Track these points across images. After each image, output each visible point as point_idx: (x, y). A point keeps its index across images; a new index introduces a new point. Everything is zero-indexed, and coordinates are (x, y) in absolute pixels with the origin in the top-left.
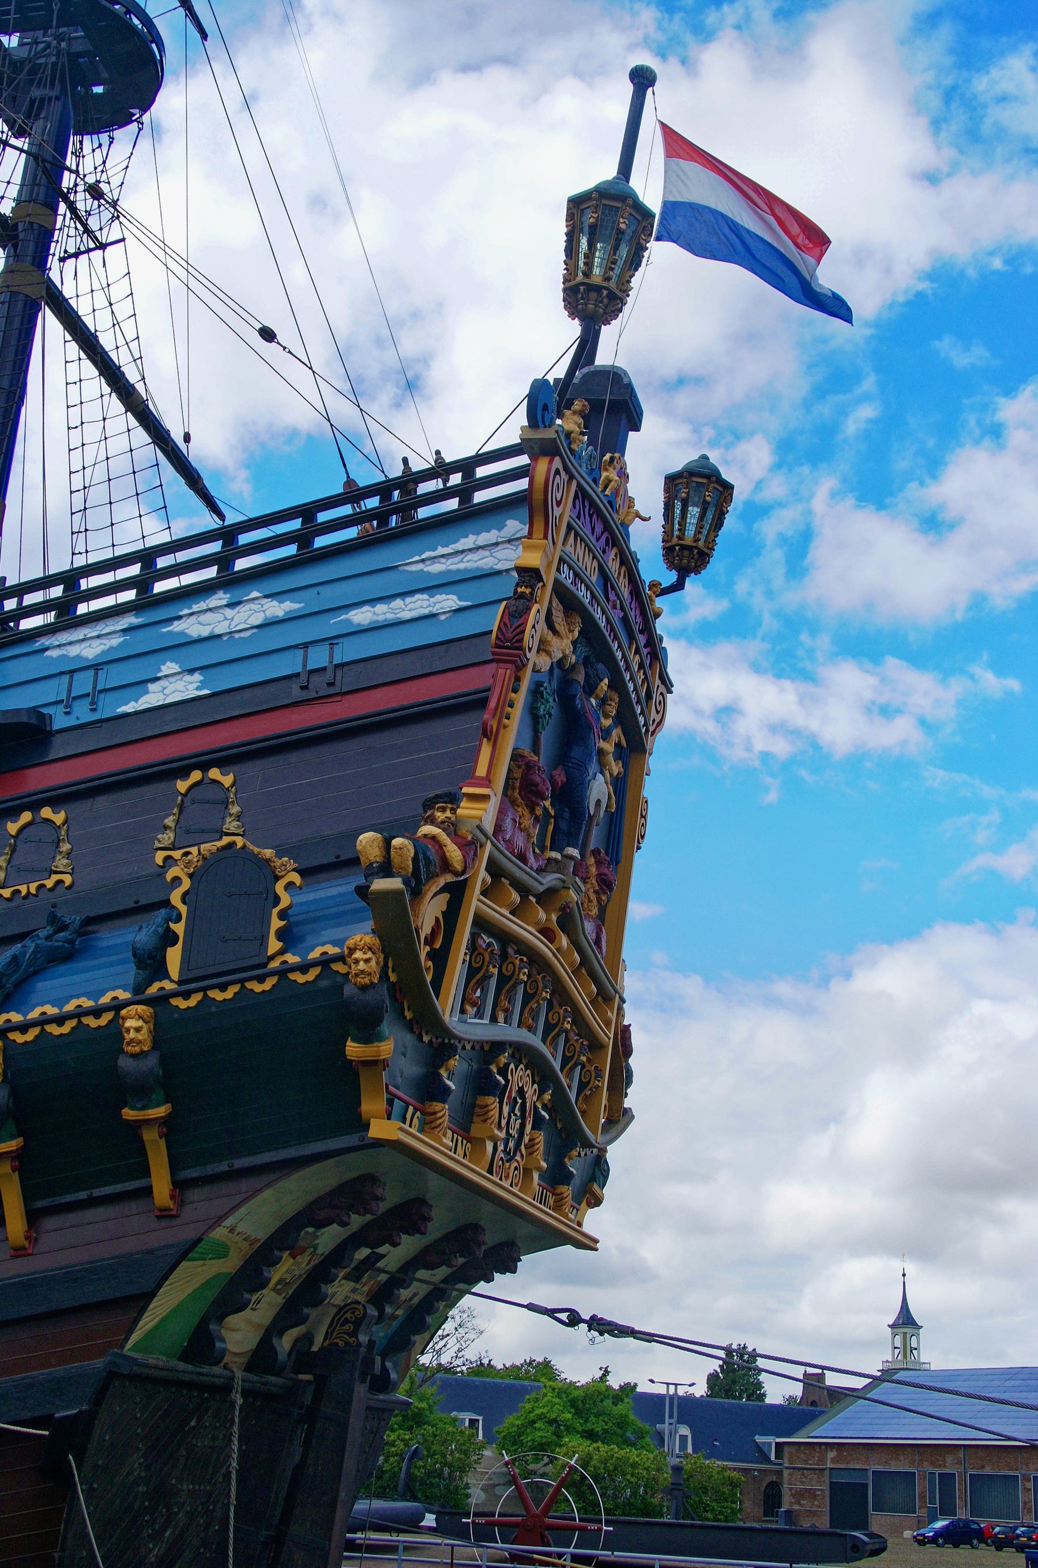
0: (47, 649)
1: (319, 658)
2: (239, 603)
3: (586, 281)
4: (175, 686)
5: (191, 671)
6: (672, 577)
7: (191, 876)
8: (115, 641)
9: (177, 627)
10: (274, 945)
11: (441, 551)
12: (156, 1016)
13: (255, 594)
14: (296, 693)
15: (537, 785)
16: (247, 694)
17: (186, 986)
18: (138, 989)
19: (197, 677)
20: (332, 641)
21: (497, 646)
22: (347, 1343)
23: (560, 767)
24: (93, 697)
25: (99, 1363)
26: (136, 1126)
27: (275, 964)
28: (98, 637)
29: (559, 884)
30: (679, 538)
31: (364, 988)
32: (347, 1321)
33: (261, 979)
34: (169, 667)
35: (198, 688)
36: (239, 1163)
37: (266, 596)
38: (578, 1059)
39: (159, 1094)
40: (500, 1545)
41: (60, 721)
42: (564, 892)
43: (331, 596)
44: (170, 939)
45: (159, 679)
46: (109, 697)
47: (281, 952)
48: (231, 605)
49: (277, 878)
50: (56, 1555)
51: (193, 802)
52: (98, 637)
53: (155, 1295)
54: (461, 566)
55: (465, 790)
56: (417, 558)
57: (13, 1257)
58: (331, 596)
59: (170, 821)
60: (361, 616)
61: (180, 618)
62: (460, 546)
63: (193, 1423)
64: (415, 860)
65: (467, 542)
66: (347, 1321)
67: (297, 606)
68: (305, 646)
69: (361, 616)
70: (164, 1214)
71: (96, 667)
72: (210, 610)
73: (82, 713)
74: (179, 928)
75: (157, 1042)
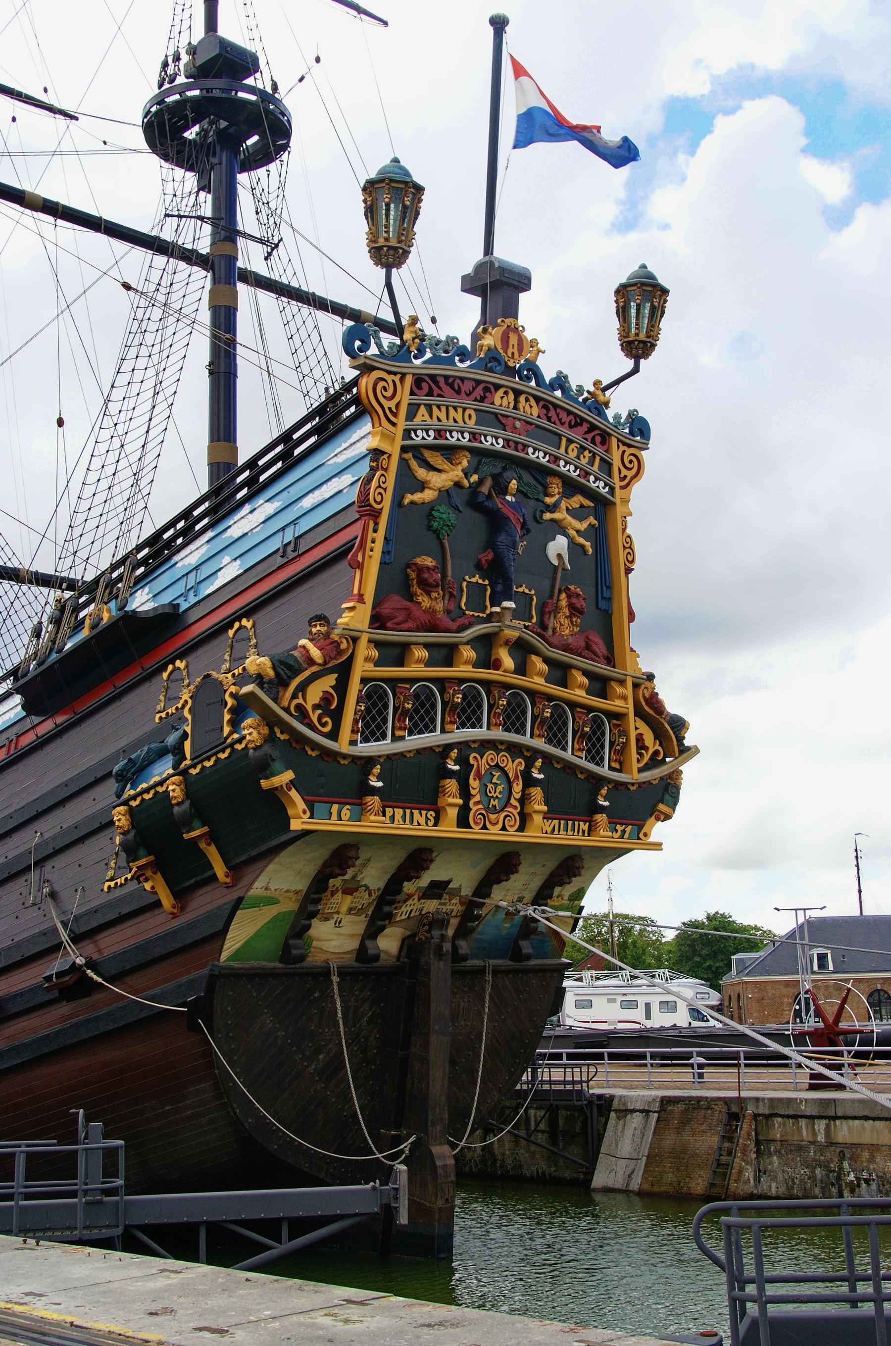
0: (176, 563)
1: (289, 536)
2: (255, 509)
3: (388, 244)
4: (231, 571)
5: (235, 559)
6: (630, 364)
7: (191, 697)
8: (205, 548)
9: (229, 533)
10: (227, 730)
11: (344, 446)
12: (185, 780)
13: (261, 501)
14: (280, 561)
15: (426, 580)
16: (259, 567)
17: (197, 759)
18: (175, 767)
19: (238, 562)
20: (294, 522)
21: (360, 507)
22: (426, 938)
23: (490, 550)
24: (195, 588)
25: (205, 971)
26: (194, 841)
27: (229, 741)
28: (197, 549)
29: (497, 629)
30: (637, 335)
31: (256, 748)
32: (425, 924)
33: (223, 751)
34: (226, 559)
35: (238, 570)
36: (254, 853)
37: (267, 501)
38: (583, 730)
39: (197, 823)
40: (811, 1048)
41: (184, 606)
42: (501, 634)
43: (296, 491)
44: (185, 735)
45: (222, 568)
46: (202, 585)
47: (231, 733)
48: (252, 512)
49: (225, 691)
50: (216, 1072)
51: (237, 641)
52: (197, 549)
53: (227, 931)
54: (353, 454)
55: (344, 606)
56: (333, 455)
57: (173, 918)
58: (296, 491)
59: (227, 657)
60: (307, 503)
61: (230, 527)
62: (351, 441)
63: (316, 995)
64: (274, 668)
65: (355, 437)
66: (425, 924)
67: (280, 503)
68: (283, 529)
69: (307, 503)
70: (228, 887)
71: (196, 568)
72: (242, 518)
73: (193, 600)
74: (188, 729)
75: (188, 794)
